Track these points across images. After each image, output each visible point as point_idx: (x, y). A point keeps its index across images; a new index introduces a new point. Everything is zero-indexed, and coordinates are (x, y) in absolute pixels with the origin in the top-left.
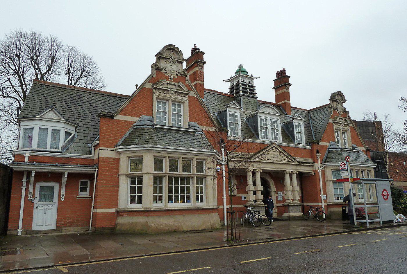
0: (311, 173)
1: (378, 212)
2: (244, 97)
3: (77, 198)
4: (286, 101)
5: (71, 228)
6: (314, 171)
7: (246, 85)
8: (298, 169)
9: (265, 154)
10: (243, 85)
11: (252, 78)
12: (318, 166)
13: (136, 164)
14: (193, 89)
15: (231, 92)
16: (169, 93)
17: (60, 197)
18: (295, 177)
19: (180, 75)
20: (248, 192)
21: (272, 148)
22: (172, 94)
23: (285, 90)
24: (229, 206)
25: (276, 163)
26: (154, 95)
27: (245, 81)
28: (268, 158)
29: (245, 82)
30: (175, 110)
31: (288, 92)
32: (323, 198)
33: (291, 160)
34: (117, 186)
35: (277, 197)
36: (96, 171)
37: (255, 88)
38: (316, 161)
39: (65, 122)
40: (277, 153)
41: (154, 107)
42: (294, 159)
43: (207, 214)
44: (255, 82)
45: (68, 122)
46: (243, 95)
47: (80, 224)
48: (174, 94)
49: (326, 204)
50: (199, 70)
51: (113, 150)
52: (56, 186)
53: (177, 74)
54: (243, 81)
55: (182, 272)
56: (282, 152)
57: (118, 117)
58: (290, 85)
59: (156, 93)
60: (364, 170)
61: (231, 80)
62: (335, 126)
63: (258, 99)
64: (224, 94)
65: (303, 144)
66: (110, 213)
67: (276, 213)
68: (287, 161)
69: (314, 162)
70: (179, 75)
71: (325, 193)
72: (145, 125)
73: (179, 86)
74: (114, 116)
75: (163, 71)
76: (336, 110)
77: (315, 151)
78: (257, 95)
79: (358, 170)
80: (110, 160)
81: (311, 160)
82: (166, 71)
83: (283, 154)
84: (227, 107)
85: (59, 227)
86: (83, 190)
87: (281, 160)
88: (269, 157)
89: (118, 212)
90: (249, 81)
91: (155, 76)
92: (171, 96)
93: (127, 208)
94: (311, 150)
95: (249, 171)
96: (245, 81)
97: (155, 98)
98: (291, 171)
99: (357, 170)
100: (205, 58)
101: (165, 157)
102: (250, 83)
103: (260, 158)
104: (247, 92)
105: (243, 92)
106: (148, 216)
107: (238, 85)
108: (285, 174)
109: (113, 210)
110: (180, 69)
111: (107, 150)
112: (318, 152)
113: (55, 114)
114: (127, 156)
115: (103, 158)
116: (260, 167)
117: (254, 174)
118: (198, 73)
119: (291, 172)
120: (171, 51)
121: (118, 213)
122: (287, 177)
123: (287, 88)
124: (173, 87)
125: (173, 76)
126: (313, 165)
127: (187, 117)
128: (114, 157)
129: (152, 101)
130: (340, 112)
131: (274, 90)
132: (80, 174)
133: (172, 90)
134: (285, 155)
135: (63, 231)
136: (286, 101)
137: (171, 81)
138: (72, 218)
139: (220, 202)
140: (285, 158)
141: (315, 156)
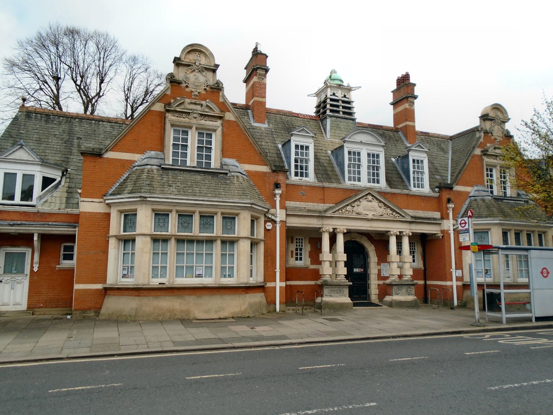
0: (437, 235)
1: (526, 300)
2: (333, 119)
3: (57, 269)
4: (408, 123)
5: (48, 309)
6: (443, 232)
7: (337, 101)
8: (408, 230)
9: (353, 205)
10: (332, 100)
11: (349, 89)
12: (449, 225)
13: (131, 221)
14: (232, 110)
15: (317, 112)
16: (190, 117)
17: (32, 267)
18: (340, 240)
19: (211, 90)
20: (322, 262)
21: (367, 195)
22: (195, 118)
23: (407, 105)
24: (283, 284)
25: (372, 220)
26: (167, 120)
27: (336, 95)
28: (358, 211)
29: (336, 96)
30: (200, 141)
31: (412, 108)
32: (455, 273)
33: (398, 215)
34: (106, 252)
35: (379, 271)
36: (77, 231)
37: (354, 105)
38: (445, 216)
39: (40, 163)
40: (375, 203)
41: (166, 139)
42: (405, 213)
43: (237, 296)
44: (353, 96)
45: (44, 163)
46: (331, 116)
47: (60, 305)
48: (199, 118)
49: (460, 283)
50: (258, 81)
51: (101, 202)
52: (28, 251)
53: (206, 87)
54: (334, 94)
55: (210, 376)
56: (384, 201)
57: (110, 155)
58: (416, 97)
59: (170, 117)
60: (533, 232)
61: (318, 94)
62: (486, 159)
63: (357, 121)
64: (304, 115)
65: (426, 190)
66: (93, 290)
67: (377, 295)
68: (391, 215)
69: (442, 218)
70: (208, 89)
71: (459, 266)
72: (147, 165)
73: (207, 106)
74: (102, 153)
75: (184, 85)
76: (490, 134)
77: (444, 200)
78: (356, 116)
79: (521, 231)
80: (96, 215)
81: (437, 215)
82: (187, 84)
83: (385, 205)
84: (292, 135)
85: (31, 307)
86: (69, 257)
87: (380, 214)
88: (360, 209)
89: (106, 289)
90: (343, 94)
91: (169, 92)
92: (194, 121)
93: (148, 284)
94: (439, 199)
95: (392, 235)
96: (336, 95)
97: (168, 126)
98: (400, 232)
99: (541, 232)
100: (269, 63)
101: (216, 214)
102: (345, 96)
103: (343, 211)
104: (338, 112)
105: (331, 111)
106: (140, 296)
107: (325, 102)
108: (388, 237)
109: (99, 286)
110: (211, 80)
111: (92, 202)
112: (449, 201)
113: (26, 153)
114: (118, 210)
115: (86, 213)
116: (342, 225)
117: (399, 238)
118: (257, 85)
119: (398, 234)
120: (197, 53)
121: (107, 291)
122: (393, 241)
123: (410, 102)
124: (199, 107)
125: (199, 91)
126: (440, 222)
127: (219, 152)
128: (102, 211)
129: (164, 129)
130: (496, 137)
131: (392, 106)
132: (64, 235)
133: (195, 111)
134: (388, 207)
135: (36, 313)
136: (408, 123)
137: (195, 99)
138: (49, 295)
139: (269, 275)
140: (389, 211)
141: (444, 209)
